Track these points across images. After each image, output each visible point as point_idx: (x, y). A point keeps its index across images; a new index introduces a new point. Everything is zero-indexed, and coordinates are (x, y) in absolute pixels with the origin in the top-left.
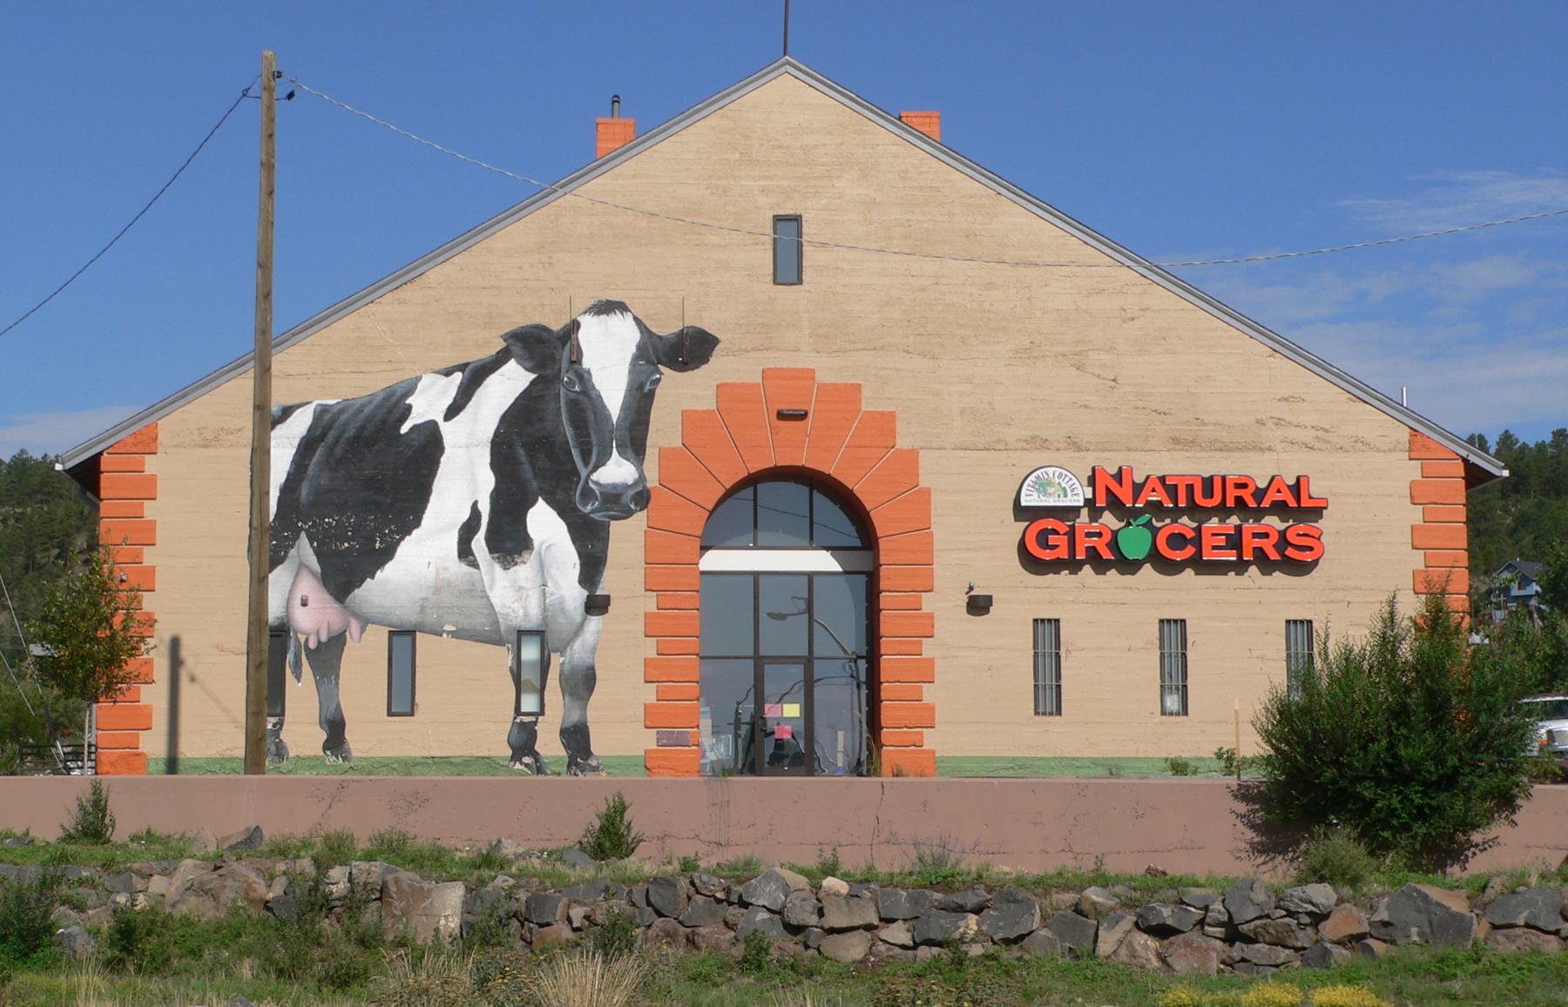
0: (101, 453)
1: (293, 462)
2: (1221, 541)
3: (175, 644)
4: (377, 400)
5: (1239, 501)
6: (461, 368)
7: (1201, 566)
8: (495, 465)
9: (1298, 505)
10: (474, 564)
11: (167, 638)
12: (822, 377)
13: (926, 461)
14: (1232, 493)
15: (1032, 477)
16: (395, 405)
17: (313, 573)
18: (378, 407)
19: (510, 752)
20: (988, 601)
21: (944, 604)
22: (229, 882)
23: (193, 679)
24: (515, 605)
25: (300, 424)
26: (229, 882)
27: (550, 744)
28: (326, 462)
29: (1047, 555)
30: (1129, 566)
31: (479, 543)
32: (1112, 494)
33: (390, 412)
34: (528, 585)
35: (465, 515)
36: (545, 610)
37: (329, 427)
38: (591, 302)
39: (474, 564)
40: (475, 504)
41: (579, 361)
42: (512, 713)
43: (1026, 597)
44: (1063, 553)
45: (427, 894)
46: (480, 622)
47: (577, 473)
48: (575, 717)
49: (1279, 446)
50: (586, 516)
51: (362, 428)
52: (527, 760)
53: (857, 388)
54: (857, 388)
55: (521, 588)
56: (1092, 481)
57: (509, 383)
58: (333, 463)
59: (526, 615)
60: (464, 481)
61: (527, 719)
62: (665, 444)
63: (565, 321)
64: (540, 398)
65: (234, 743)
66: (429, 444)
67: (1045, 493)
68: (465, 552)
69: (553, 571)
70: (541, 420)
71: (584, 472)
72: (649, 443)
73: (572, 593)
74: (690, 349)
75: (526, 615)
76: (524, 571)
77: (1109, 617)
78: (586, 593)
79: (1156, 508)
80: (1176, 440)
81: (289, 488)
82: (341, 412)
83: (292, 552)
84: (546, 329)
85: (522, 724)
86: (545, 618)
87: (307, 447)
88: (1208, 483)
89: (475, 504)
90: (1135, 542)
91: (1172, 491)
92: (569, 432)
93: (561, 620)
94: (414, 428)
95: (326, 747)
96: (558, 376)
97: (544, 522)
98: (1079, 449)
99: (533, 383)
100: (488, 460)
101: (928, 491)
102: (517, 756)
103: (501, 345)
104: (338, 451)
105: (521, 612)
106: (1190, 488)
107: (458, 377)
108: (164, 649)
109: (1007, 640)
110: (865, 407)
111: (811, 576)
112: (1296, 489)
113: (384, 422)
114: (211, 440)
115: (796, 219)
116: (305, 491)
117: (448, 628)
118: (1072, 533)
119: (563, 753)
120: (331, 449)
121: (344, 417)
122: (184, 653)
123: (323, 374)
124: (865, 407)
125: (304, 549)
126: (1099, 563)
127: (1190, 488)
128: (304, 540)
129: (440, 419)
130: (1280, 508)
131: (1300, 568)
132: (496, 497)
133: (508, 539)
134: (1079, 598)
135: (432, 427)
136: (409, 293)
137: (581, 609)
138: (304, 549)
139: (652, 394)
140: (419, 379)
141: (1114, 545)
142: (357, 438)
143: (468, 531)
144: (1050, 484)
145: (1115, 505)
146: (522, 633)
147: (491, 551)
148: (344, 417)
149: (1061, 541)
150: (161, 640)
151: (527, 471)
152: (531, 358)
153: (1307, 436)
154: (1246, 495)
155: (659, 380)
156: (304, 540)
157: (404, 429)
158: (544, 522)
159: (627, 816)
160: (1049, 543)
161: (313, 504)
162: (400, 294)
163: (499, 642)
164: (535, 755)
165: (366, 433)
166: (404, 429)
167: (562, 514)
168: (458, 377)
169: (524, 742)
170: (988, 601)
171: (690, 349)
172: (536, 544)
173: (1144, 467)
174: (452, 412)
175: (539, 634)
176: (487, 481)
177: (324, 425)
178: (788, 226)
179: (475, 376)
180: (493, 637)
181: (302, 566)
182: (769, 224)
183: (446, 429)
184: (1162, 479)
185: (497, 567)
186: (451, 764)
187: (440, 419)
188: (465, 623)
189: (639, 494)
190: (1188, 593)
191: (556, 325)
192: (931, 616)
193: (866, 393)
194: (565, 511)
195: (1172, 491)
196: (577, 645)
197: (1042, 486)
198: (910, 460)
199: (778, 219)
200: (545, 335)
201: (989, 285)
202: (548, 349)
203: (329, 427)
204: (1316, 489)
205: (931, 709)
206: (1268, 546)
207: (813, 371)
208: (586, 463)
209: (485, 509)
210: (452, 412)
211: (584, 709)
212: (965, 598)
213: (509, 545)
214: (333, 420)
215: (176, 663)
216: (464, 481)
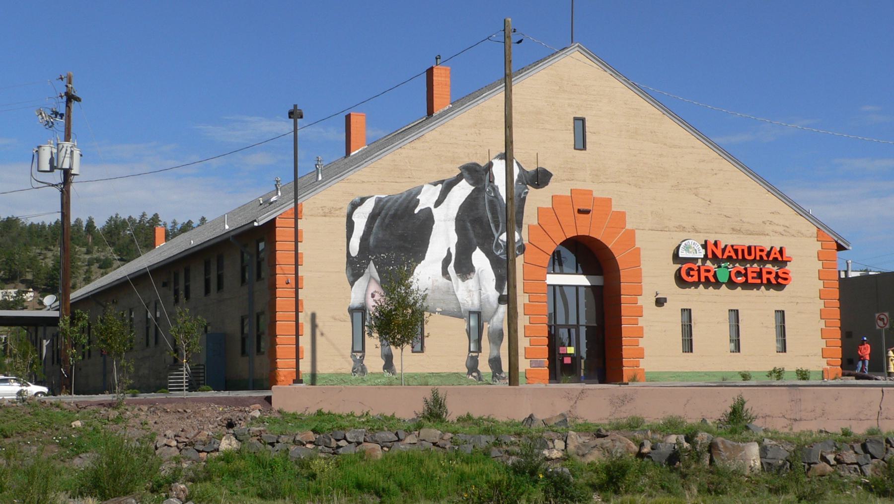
0: (275, 219)
1: (366, 225)
2: (755, 275)
3: (313, 316)
4: (404, 196)
5: (761, 257)
6: (442, 182)
7: (746, 285)
8: (457, 230)
9: (779, 259)
10: (449, 279)
11: (309, 313)
12: (596, 194)
13: (638, 234)
14: (758, 254)
15: (683, 244)
16: (411, 199)
17: (376, 281)
18: (404, 200)
19: (466, 371)
20: (665, 300)
21: (646, 301)
22: (618, 444)
23: (322, 334)
24: (468, 299)
25: (368, 207)
26: (618, 444)
27: (484, 367)
28: (381, 225)
29: (689, 279)
30: (717, 284)
31: (451, 268)
32: (715, 254)
33: (410, 202)
34: (473, 289)
35: (445, 255)
36: (481, 301)
37: (382, 209)
38: (498, 153)
39: (449, 279)
40: (449, 249)
41: (493, 182)
42: (350, 351)
43: (680, 298)
44: (695, 279)
45: (742, 449)
46: (452, 307)
47: (493, 236)
48: (495, 354)
49: (771, 234)
50: (497, 256)
51: (397, 210)
52: (474, 374)
53: (610, 200)
54: (610, 200)
55: (470, 291)
56: (705, 246)
57: (463, 190)
58: (384, 227)
59: (473, 304)
60: (443, 238)
61: (474, 354)
62: (530, 223)
63: (487, 162)
64: (477, 198)
65: (346, 366)
66: (427, 219)
67: (689, 252)
68: (445, 273)
69: (484, 283)
70: (477, 209)
71: (496, 236)
72: (524, 222)
73: (492, 294)
74: (540, 178)
75: (473, 304)
76: (471, 283)
77: (711, 306)
78: (498, 294)
79: (730, 259)
80: (733, 229)
81: (364, 239)
82: (387, 201)
83: (367, 271)
84: (478, 165)
85: (472, 357)
86: (481, 305)
87: (372, 218)
88: (749, 248)
89: (449, 249)
90: (723, 276)
91: (736, 251)
92: (490, 216)
93: (488, 306)
94: (421, 211)
95: (384, 368)
96: (484, 188)
97: (479, 258)
98: (697, 232)
99: (473, 191)
100: (454, 228)
101: (639, 249)
102: (470, 373)
103: (458, 172)
104: (387, 221)
105: (470, 303)
106: (743, 250)
107: (440, 186)
108: (309, 319)
109: (671, 317)
110: (613, 209)
111: (577, 287)
112: (781, 251)
113: (407, 207)
114: (328, 213)
115: (583, 120)
116: (372, 240)
117: (439, 310)
118: (699, 271)
119: (490, 371)
120: (383, 219)
121: (389, 204)
122: (318, 321)
123: (375, 181)
124: (613, 209)
125: (372, 269)
126: (707, 283)
127: (743, 250)
128: (372, 264)
129: (432, 207)
130: (775, 261)
131: (779, 287)
132: (458, 245)
133: (465, 268)
134: (700, 299)
135: (429, 209)
136: (418, 144)
137: (496, 301)
138: (372, 269)
139: (524, 198)
140: (422, 187)
141: (715, 276)
142: (394, 216)
143: (446, 262)
144: (690, 247)
145: (715, 259)
146: (470, 312)
147: (457, 272)
148: (389, 204)
149: (695, 273)
150: (306, 314)
151: (471, 234)
152: (472, 179)
153: (780, 229)
154: (764, 254)
155: (527, 193)
156: (372, 264)
157: (416, 211)
158: (479, 258)
159: (746, 406)
160: (688, 275)
161: (376, 247)
162: (413, 145)
163: (461, 317)
164: (478, 372)
165: (399, 212)
166: (416, 211)
167: (488, 255)
168: (440, 186)
169: (473, 366)
170: (665, 300)
171: (540, 178)
172: (476, 269)
173: (728, 239)
174: (438, 203)
175: (479, 314)
176: (454, 238)
177: (380, 207)
178: (580, 122)
179: (448, 186)
180: (458, 314)
181: (371, 277)
182: (572, 121)
183: (435, 211)
184: (732, 246)
185: (459, 280)
186: (441, 376)
187: (432, 207)
188: (445, 307)
189: (520, 246)
190: (740, 298)
191: (483, 163)
192: (641, 307)
193: (614, 203)
194: (489, 254)
195: (736, 251)
196: (495, 318)
197: (687, 248)
198: (631, 234)
199: (575, 119)
200: (478, 168)
201: (661, 155)
202: (477, 174)
203: (382, 209)
204: (787, 253)
205: (642, 349)
206: (772, 277)
207: (591, 191)
208: (497, 231)
209: (453, 252)
210: (438, 203)
211: (499, 350)
212: (654, 299)
213: (464, 269)
214: (384, 206)
215: (314, 326)
216: (443, 238)
